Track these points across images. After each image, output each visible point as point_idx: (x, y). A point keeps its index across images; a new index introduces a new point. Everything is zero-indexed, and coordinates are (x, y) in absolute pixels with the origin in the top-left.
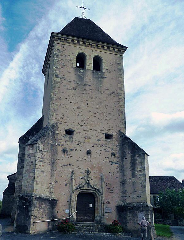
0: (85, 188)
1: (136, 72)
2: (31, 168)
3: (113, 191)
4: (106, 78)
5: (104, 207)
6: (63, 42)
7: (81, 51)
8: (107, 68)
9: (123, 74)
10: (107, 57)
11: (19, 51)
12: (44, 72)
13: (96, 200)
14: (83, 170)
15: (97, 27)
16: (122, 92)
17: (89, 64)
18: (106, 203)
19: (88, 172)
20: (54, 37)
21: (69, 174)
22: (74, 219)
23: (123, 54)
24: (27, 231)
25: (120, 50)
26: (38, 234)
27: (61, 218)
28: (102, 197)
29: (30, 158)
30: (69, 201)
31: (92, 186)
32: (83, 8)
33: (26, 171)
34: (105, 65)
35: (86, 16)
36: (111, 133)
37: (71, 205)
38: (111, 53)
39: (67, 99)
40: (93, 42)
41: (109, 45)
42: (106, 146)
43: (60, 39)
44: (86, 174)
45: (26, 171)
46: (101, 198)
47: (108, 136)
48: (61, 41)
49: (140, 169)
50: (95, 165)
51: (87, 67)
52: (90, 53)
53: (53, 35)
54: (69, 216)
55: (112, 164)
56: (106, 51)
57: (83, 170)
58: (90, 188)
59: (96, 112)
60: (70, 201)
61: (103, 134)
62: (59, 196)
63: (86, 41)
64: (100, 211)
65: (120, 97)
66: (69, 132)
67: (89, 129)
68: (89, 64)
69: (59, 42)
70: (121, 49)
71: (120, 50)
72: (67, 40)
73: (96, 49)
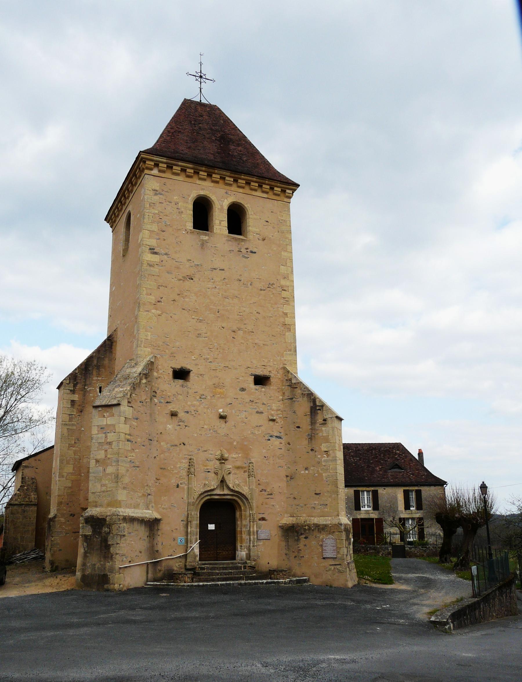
0: (218, 492)
1: (317, 225)
2: (108, 456)
3: (271, 494)
4: (255, 253)
5: (255, 529)
6: (163, 172)
7: (202, 193)
8: (258, 230)
9: (290, 244)
10: (258, 207)
11: (182, 368)
12: (111, 218)
13: (238, 514)
14: (211, 454)
15: (233, 127)
16: (288, 283)
17: (220, 219)
18: (260, 520)
19: (222, 460)
20: (145, 162)
21: (184, 464)
22: (346, 525)
23: (290, 198)
24: (106, 586)
25: (283, 191)
26: (129, 590)
27: (171, 555)
28: (251, 508)
29: (104, 435)
30: (185, 519)
31: (231, 486)
32: (201, 77)
33: (97, 461)
34: (253, 223)
35: (210, 97)
36: (267, 374)
37: (189, 528)
38: (265, 195)
39: (174, 300)
40: (228, 174)
41: (261, 181)
42: (257, 401)
43: (157, 165)
44: (218, 462)
45: (97, 461)
46: (248, 510)
47: (261, 380)
48: (160, 171)
49: (326, 450)
50: (235, 443)
51: (215, 229)
52: (222, 197)
53: (140, 152)
54: (186, 551)
55: (269, 440)
56: (254, 193)
57: (211, 454)
58: (226, 492)
59: (235, 328)
60: (187, 520)
61: (252, 375)
62: (165, 511)
63: (213, 171)
64: (248, 537)
65: (284, 294)
66: (181, 374)
67: (223, 365)
68: (220, 219)
69: (155, 172)
70: (285, 186)
71: (283, 191)
72: (172, 168)
73: (234, 188)
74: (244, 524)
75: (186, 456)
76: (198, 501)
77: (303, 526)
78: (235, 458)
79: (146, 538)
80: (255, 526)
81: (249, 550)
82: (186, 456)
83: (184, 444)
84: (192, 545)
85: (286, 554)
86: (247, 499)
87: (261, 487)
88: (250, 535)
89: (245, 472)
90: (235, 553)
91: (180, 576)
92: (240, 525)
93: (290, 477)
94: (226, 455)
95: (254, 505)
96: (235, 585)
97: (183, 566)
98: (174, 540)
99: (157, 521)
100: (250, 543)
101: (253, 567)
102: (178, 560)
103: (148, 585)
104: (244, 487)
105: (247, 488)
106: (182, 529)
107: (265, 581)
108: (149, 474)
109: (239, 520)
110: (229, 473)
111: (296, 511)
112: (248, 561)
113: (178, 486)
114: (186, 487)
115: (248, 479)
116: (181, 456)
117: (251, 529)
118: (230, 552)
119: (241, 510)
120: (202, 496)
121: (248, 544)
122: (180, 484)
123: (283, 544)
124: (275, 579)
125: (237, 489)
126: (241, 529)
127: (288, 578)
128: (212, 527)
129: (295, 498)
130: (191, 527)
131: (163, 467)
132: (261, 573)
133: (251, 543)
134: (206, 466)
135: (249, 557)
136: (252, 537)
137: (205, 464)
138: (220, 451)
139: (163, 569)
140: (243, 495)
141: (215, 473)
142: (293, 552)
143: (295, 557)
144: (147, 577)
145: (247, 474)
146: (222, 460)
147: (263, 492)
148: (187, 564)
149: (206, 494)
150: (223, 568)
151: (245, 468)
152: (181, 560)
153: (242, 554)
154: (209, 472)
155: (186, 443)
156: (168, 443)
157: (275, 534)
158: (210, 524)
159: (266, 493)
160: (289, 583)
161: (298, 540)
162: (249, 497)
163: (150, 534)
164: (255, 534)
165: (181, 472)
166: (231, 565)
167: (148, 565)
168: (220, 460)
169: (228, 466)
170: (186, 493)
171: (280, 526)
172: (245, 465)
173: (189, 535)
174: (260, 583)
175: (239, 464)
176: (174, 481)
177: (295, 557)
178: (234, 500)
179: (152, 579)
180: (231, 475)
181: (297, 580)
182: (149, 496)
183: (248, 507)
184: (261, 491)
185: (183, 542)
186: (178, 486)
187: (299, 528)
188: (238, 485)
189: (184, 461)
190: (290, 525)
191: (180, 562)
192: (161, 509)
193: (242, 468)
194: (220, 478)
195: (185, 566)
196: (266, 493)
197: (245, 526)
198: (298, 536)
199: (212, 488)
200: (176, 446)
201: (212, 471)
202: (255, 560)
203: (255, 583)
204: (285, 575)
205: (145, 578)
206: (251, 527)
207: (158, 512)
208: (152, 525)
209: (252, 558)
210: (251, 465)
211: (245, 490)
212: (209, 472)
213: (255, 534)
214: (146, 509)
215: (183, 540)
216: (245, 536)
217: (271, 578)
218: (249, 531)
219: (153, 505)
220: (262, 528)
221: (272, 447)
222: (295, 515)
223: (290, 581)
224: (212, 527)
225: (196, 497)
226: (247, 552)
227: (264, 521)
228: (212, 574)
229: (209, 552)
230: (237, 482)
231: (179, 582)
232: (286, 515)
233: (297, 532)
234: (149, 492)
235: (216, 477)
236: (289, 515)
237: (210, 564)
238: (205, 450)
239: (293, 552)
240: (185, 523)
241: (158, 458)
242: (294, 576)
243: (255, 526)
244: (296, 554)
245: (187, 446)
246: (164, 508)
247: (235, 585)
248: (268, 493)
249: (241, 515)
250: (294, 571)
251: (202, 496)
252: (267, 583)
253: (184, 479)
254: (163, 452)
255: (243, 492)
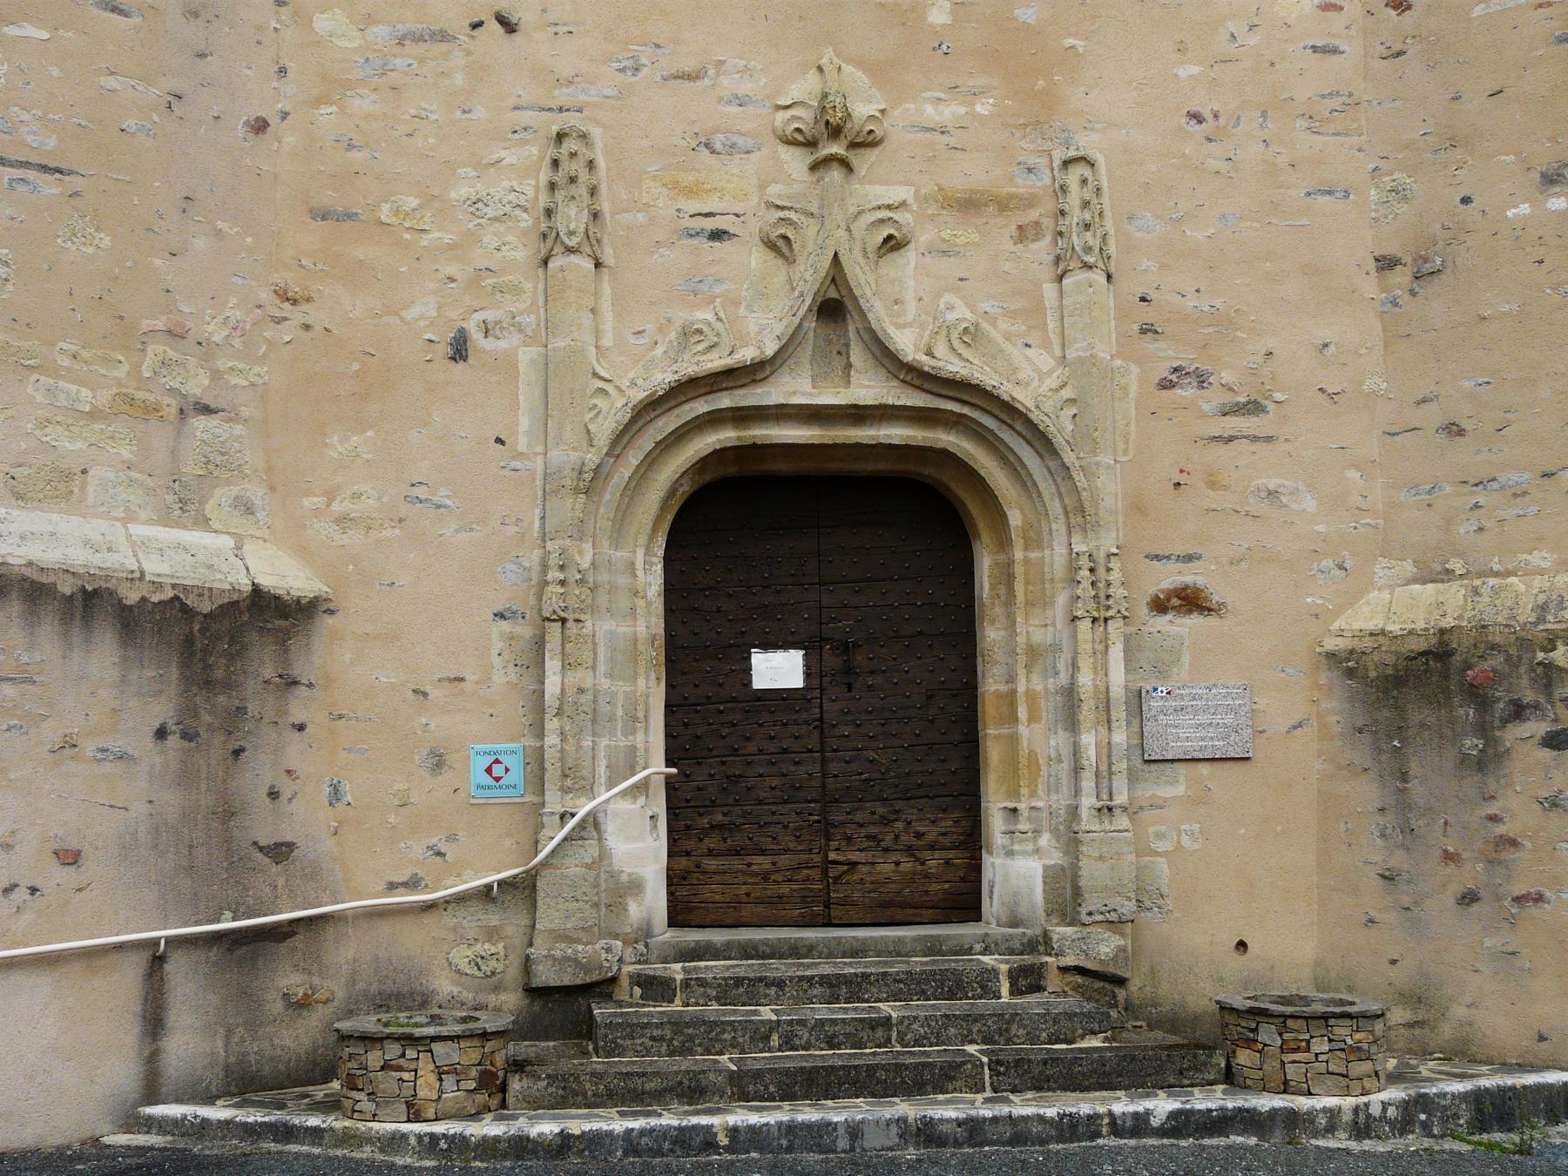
3: (1254, 407)
13: (985, 563)
18: (1160, 606)
19: (833, 141)
21: (517, 176)
27: (413, 884)
28: (1080, 515)
31: (906, 344)
37: (552, 665)
44: (795, 162)
46: (1059, 527)
58: (869, 388)
64: (1059, 741)
74: (1035, 641)
75: (528, 117)
76: (633, 458)
77: (1526, 644)
78: (937, 129)
79: (140, 743)
80: (1116, 653)
81: (1072, 841)
82: (528, 117)
83: (508, 26)
84: (569, 803)
85: (1388, 878)
86: (1041, 441)
87: (1165, 354)
88: (1073, 726)
89: (1024, 234)
90: (976, 868)
91: (374, 1058)
92: (1000, 655)
93: (1413, 267)
94: (862, 109)
95: (1107, 486)
96: (872, 1140)
97: (513, 972)
98: (438, 763)
99: (272, 616)
100: (1077, 792)
101: (1102, 981)
102: (472, 920)
103: (150, 1124)
104: (1016, 354)
105: (1044, 361)
106: (499, 679)
107: (1162, 1106)
108: (200, 244)
109: (998, 610)
110: (892, 245)
111: (1465, 528)
112: (1061, 932)
113: (460, 350)
114: (527, 356)
115: (1049, 290)
116: (480, 113)
117: (1085, 679)
118: (934, 862)
119: (1003, 541)
120: (669, 423)
121: (1061, 800)
122: (476, 335)
123: (1366, 793)
124: (1264, 1088)
125: (953, 366)
126: (1011, 679)
127: (1395, 1078)
128: (777, 669)
129: (1454, 430)
130: (566, 666)
131: (328, 198)
132: (1171, 1023)
133: (1088, 784)
134: (690, 192)
135: (1066, 896)
136: (1088, 740)
137: (688, 178)
138: (812, 77)
139: (335, 987)
140: (1010, 412)
141: (771, 245)
142: (1449, 857)
143: (1469, 898)
144: (152, 1062)
145: (1042, 249)
146: (833, 141)
147: (1186, 393)
148: (536, 952)
149: (701, 407)
150: (825, 980)
151: (1029, 202)
152: (494, 920)
153: (1016, 872)
154: (717, 235)
155: (523, 14)
156: (370, 19)
157: (1299, 719)
158: (768, 645)
159: (1212, 399)
160: (1403, 1125)
161: (1488, 761)
162: (1060, 427)
163: (189, 710)
164: (1119, 713)
165: (490, 240)
166: (918, 962)
167: (158, 961)
168: (811, 144)
169: (879, 186)
170: (527, 394)
171: (1331, 656)
172: (1023, 185)
173: (552, 725)
174: (1117, 1127)
175: (972, 173)
176: (426, 312)
177: (1469, 898)
178: (946, 457)
179: (215, 1078)
180: (910, 256)
181: (1477, 1097)
182: (200, 423)
183: (1055, 507)
184: (1166, 385)
185: (515, 777)
186: (460, 350)
187: (1497, 661)
188: (971, 336)
189: (510, 157)
190: (1420, 645)
191: (492, 934)
192: (323, 529)
193: (1004, 205)
194: (809, 275)
195: (527, 962)
196: (1212, 399)
197: (1033, 652)
198: (1483, 730)
199: (747, 355)
200: (443, 36)
201: (750, 230)
202: (1115, 924)
203: (1070, 1128)
204: (1357, 1052)
205: (120, 1071)
206: (1085, 665)
207: (304, 553)
208: (222, 648)
209: (1092, 902)
210: (1073, 177)
211: (1028, 376)
212: (717, 235)
213: (1119, 713)
214: (165, 520)
215: (514, 762)
216: (1039, 737)
217: (1230, 1078)
218: (1070, 694)
219: (256, 492)
220: (1182, 672)
221: (1253, 40)
222: (1457, 566)
223: (1407, 1106)
224: (777, 669)
225: (605, 429)
226: (1056, 858)
227: (1195, 620)
228: (711, 1035)
229: (762, 863)
230: (961, 313)
231: (366, 1105)
232: (1381, 570)
233: (1478, 695)
234: (198, 385)
235: (778, 271)
236: (1408, 567)
237: (747, 951)
238: (688, 65)
239: (1449, 857)
240: (525, 630)
241: (287, 137)
242: (1461, 1054)
243: (1116, 653)
244: (1473, 873)
245: (533, 43)
246: (343, 520)
247: (872, 1140)
248: (1228, 398)
249: (1007, 576)
250: (1459, 1011)
251: (669, 423)
252: (1181, 1124)
253: (516, 290)
254: (333, 89)
255: (1007, 390)
